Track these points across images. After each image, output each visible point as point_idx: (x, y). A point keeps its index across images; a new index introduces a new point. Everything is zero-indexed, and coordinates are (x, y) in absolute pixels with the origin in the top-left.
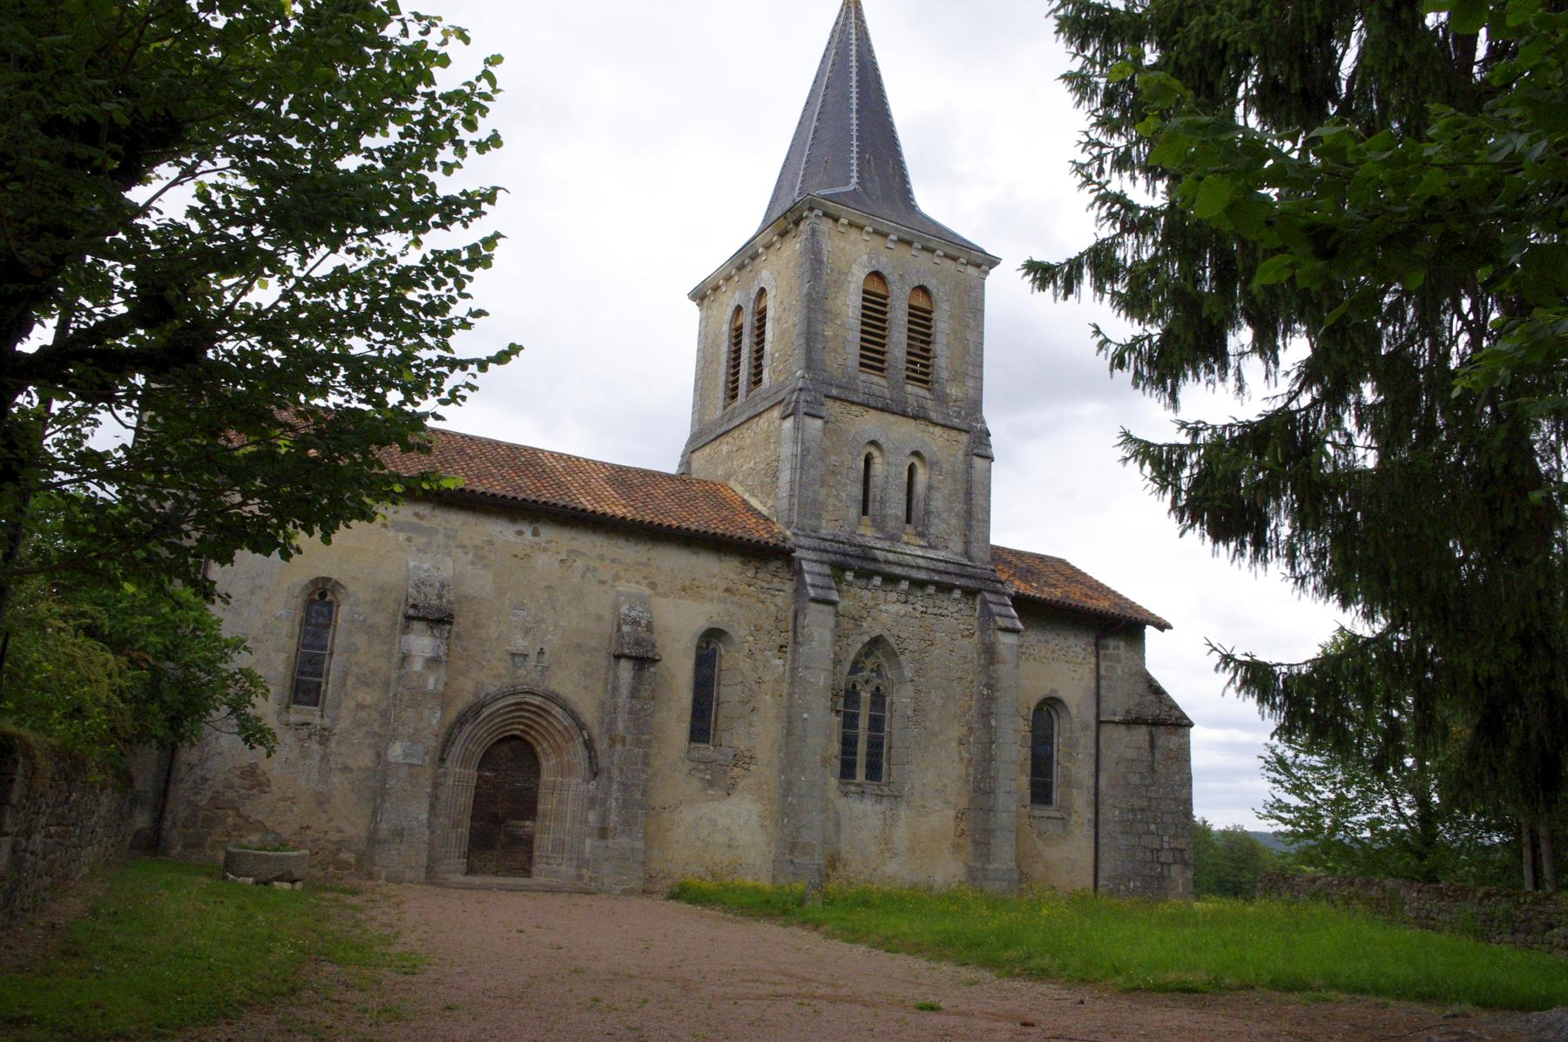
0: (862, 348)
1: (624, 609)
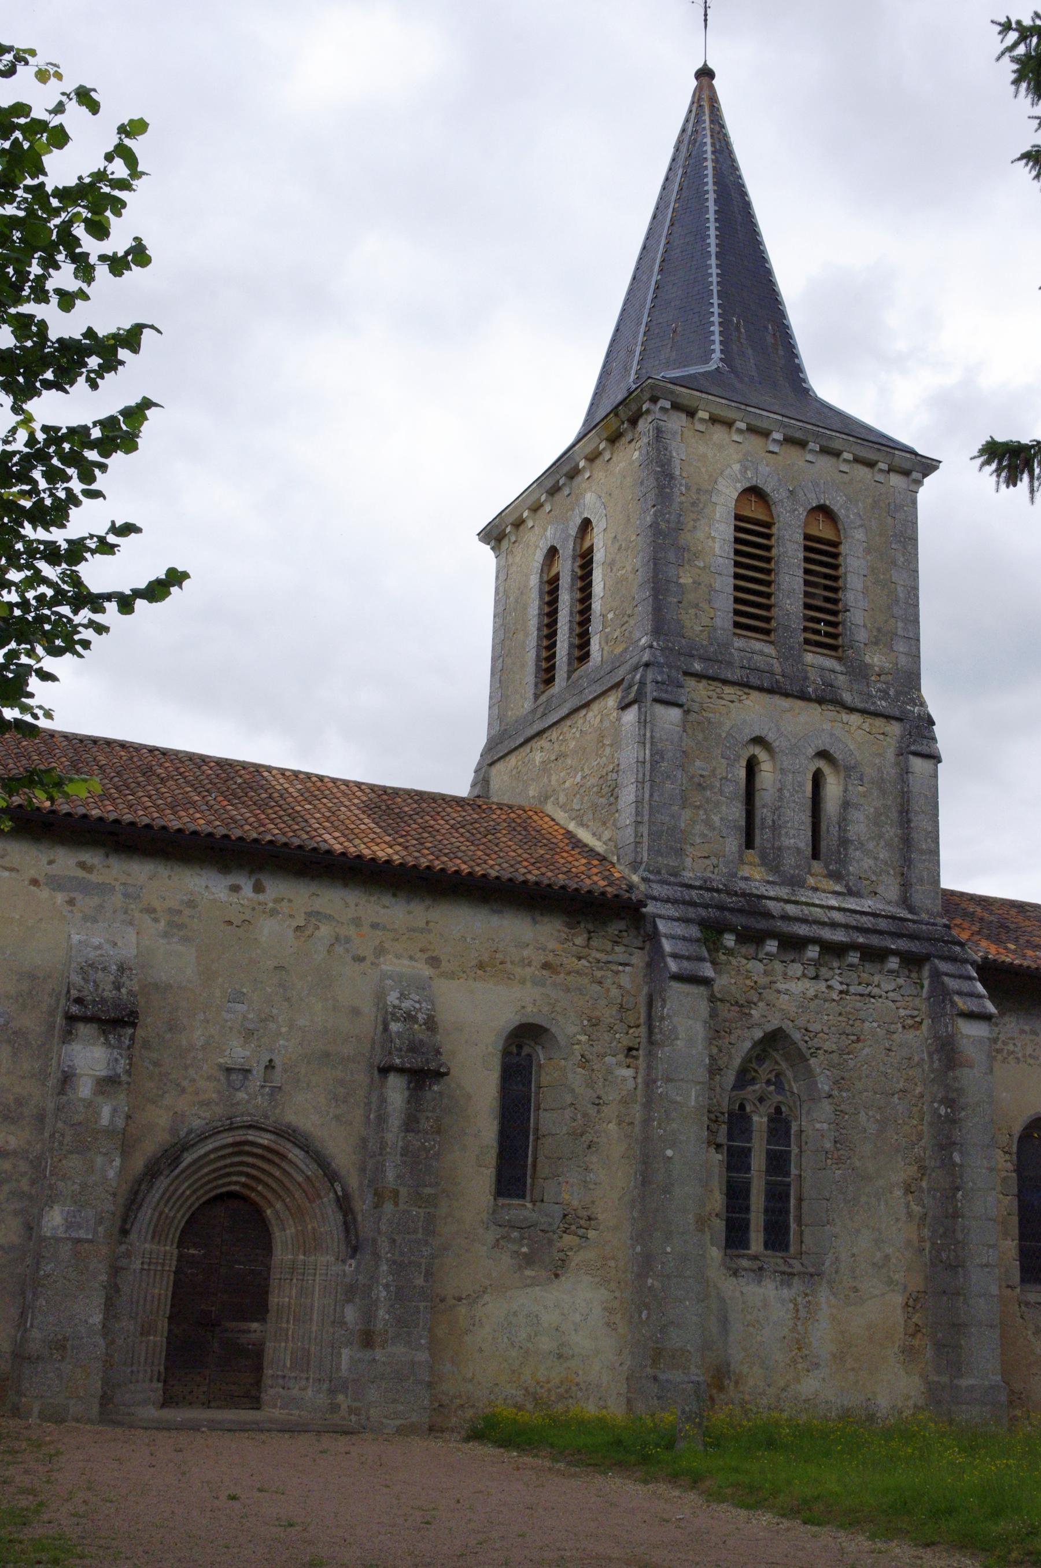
0: (737, 600)
1: (393, 998)
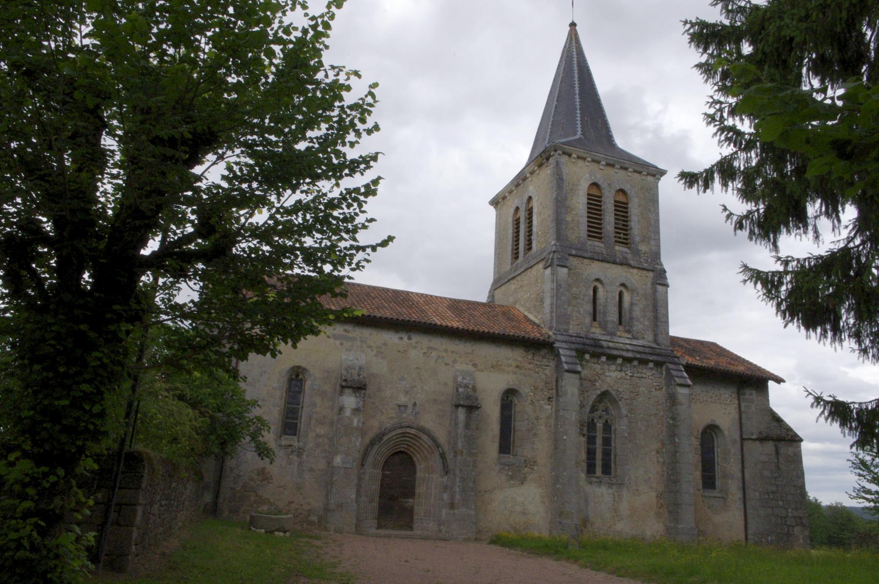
0: (589, 226)
1: (460, 379)
